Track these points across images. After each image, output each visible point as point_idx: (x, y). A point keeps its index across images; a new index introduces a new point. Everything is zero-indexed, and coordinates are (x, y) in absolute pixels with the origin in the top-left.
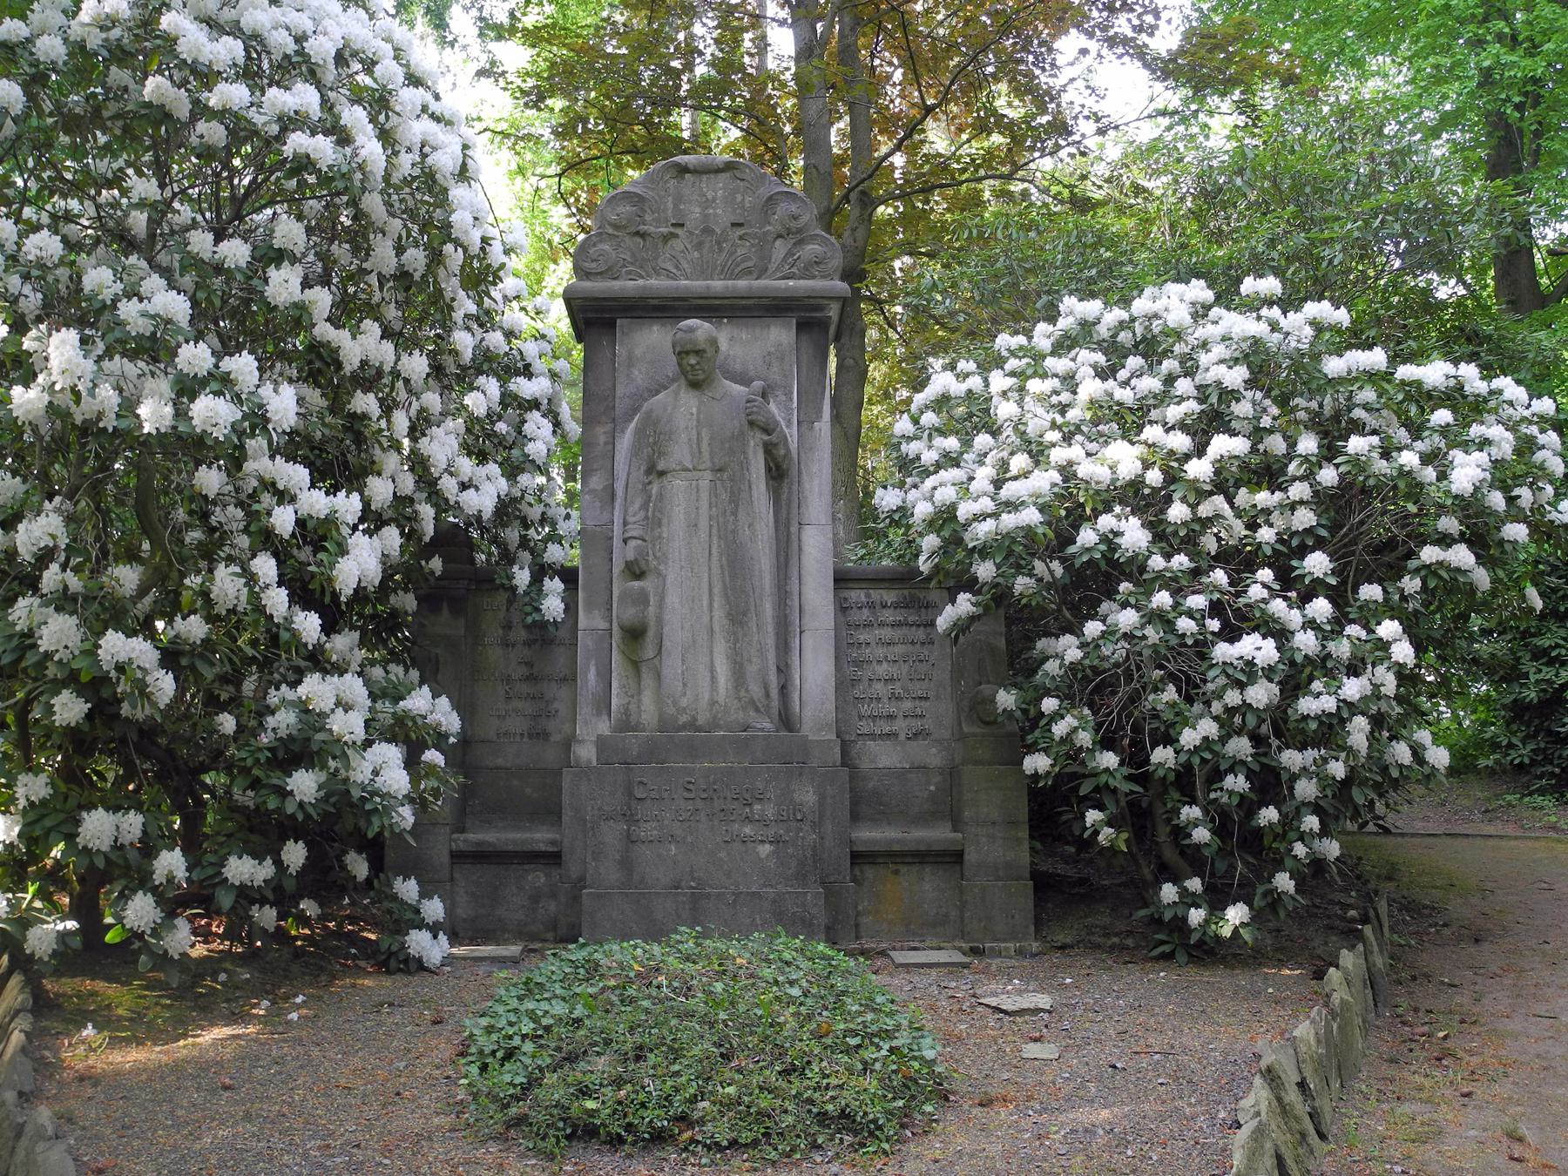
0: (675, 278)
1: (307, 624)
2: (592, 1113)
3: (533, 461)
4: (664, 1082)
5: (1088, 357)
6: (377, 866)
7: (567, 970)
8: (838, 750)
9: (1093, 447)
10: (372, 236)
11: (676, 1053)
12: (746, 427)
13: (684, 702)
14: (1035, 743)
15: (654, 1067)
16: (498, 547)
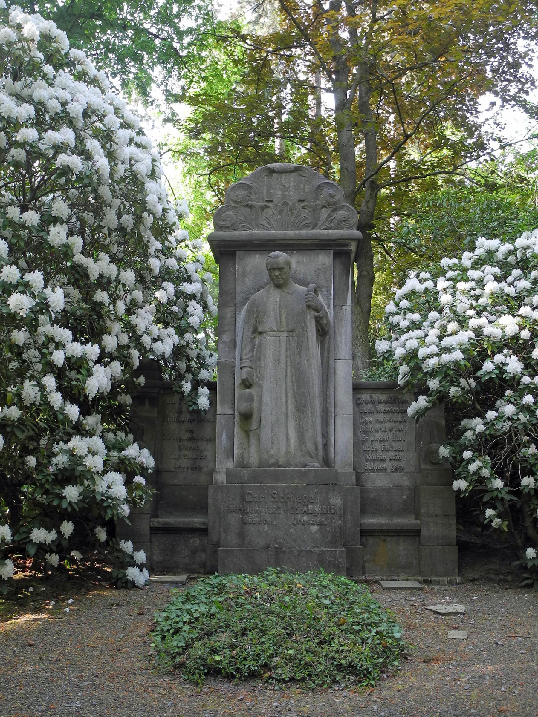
0: (267, 229)
1: (72, 411)
2: (218, 662)
3: (192, 327)
4: (256, 647)
5: (490, 270)
6: (111, 534)
7: (209, 589)
8: (354, 478)
9: (492, 318)
10: (104, 208)
11: (263, 632)
12: (306, 308)
13: (272, 452)
14: (459, 474)
15: (251, 639)
16: (175, 371)
